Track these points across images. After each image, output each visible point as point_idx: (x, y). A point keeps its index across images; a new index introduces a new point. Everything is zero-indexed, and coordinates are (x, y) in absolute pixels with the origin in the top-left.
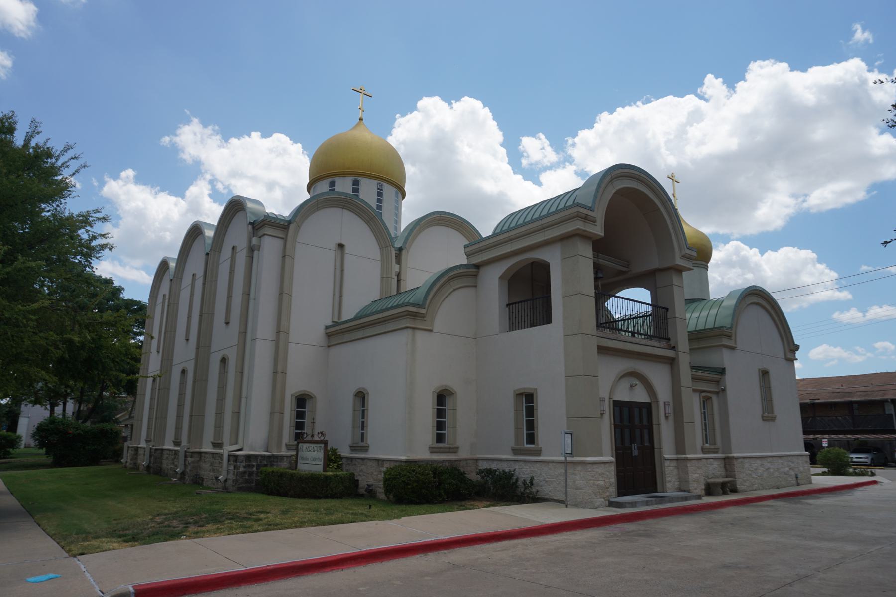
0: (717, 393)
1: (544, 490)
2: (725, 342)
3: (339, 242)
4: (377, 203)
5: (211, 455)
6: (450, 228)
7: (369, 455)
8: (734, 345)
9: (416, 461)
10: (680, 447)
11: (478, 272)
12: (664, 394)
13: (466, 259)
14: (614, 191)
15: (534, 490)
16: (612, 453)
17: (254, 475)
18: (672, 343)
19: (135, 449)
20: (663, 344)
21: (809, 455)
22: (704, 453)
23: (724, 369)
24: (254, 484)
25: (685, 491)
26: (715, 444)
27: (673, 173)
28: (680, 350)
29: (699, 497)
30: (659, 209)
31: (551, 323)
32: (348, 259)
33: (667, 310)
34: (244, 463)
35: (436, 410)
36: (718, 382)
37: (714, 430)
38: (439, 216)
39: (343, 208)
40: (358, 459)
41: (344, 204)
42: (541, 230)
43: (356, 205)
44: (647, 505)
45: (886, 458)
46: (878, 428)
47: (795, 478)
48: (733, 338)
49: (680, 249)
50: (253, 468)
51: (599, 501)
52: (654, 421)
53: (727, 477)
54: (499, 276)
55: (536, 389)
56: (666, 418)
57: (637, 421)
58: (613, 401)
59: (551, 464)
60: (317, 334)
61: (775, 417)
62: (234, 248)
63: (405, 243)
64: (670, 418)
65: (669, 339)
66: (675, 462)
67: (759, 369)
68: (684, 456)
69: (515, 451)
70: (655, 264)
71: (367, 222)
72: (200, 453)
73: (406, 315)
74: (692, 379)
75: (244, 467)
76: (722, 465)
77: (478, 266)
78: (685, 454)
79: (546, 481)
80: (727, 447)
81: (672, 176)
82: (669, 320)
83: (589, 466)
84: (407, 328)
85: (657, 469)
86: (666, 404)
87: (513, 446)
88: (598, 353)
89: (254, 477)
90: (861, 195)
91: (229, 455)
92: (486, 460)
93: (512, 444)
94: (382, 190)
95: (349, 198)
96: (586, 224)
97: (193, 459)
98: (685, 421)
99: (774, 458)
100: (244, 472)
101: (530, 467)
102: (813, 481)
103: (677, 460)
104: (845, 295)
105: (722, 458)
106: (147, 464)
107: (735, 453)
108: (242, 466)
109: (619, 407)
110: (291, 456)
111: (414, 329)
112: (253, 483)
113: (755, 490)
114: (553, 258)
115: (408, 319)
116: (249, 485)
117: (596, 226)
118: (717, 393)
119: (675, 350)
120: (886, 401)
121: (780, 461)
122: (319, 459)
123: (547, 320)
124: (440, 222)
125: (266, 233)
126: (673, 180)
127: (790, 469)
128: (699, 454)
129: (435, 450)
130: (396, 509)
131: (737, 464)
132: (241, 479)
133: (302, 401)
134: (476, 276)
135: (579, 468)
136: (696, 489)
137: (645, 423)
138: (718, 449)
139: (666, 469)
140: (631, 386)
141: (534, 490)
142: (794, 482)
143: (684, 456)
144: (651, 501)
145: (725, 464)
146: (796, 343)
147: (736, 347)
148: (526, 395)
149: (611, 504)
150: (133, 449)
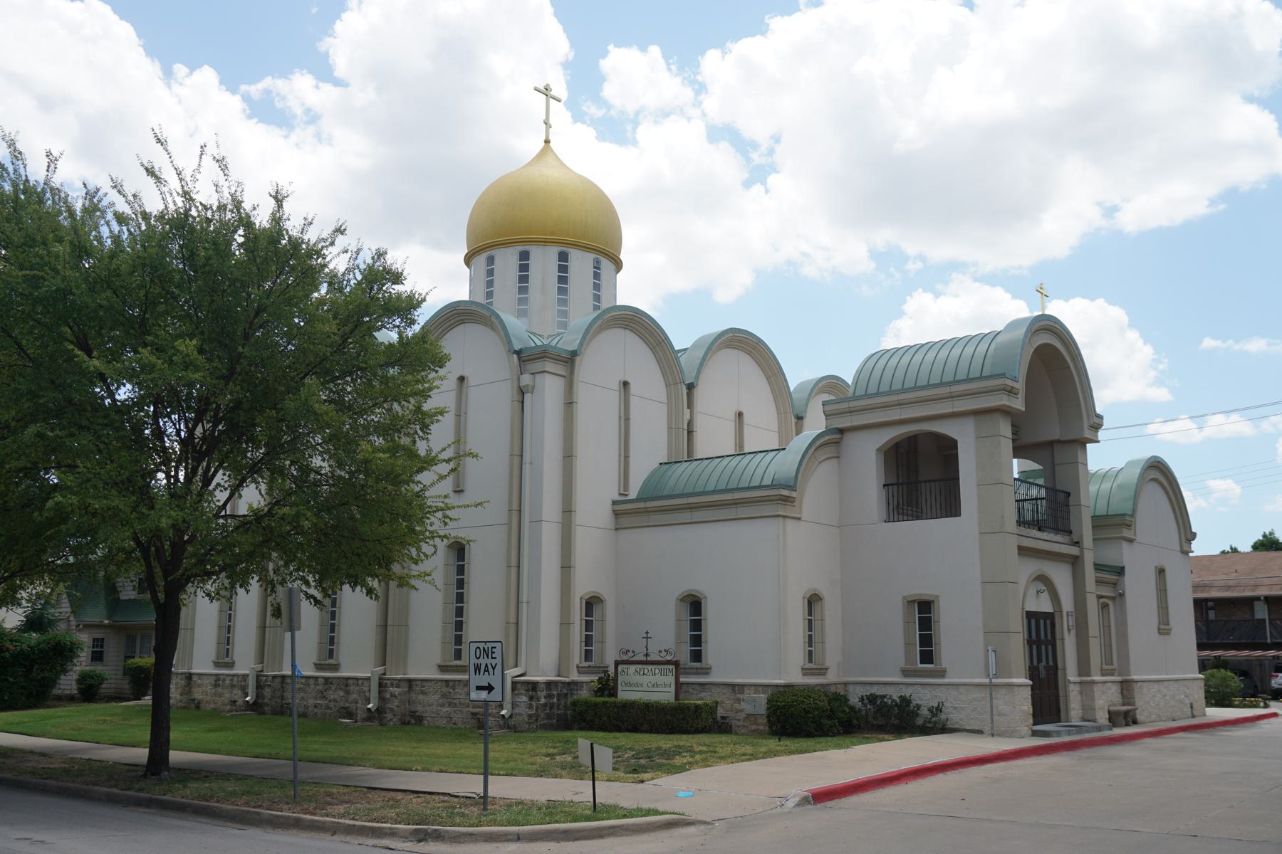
0: (1113, 598)
1: (953, 719)
2: (1126, 533)
3: (623, 379)
4: (558, 283)
5: (444, 683)
6: (740, 352)
7: (714, 678)
8: (1132, 537)
9: (792, 686)
10: (1084, 668)
11: (841, 438)
12: (1067, 604)
13: (824, 420)
14: (1033, 350)
15: (943, 717)
16: (1026, 673)
17: (555, 708)
18: (1075, 538)
19: (186, 677)
20: (1066, 539)
21: (1204, 679)
22: (1103, 675)
23: (1123, 568)
24: (555, 721)
25: (1089, 721)
26: (1112, 664)
27: (1042, 284)
28: (1085, 547)
29: (1099, 729)
30: (1069, 367)
31: (960, 516)
32: (634, 402)
33: (1069, 494)
34: (544, 693)
35: (337, 606)
36: (1115, 584)
37: (1111, 646)
38: (732, 335)
39: (625, 328)
40: (692, 684)
41: (627, 323)
42: (948, 398)
43: (641, 324)
44: (1069, 735)
45: (1256, 686)
46: (1244, 641)
47: (1190, 709)
48: (1133, 527)
49: (1088, 416)
50: (553, 698)
51: (1025, 730)
52: (1058, 636)
53: (1124, 705)
54: (877, 447)
55: (938, 596)
56: (1069, 630)
57: (1043, 637)
58: (1026, 611)
59: (961, 687)
60: (603, 514)
61: (1171, 630)
62: (462, 379)
63: (581, 344)
64: (1072, 631)
65: (1070, 532)
66: (1078, 685)
67: (1156, 567)
68: (1089, 678)
69: (905, 673)
70: (1056, 435)
71: (652, 349)
72: (410, 681)
73: (777, 500)
74: (1096, 582)
75: (545, 697)
76: (1119, 690)
77: (841, 431)
78: (1090, 675)
79: (955, 708)
80: (1125, 668)
81: (1041, 288)
82: (1071, 508)
83: (1016, 688)
84: (779, 516)
85: (1061, 693)
86: (1070, 613)
87: (903, 665)
88: (1019, 554)
89: (555, 711)
90: (1200, 208)
91: (512, 682)
92: (860, 683)
93: (902, 663)
94: (599, 268)
95: (637, 315)
96: (1011, 397)
97: (400, 689)
98: (1090, 635)
99: (1171, 682)
100: (545, 705)
101: (930, 692)
102: (1207, 714)
103: (1081, 683)
104: (1162, 394)
105: (1118, 682)
106: (253, 700)
107: (1135, 675)
108: (542, 697)
109: (1030, 616)
110: (592, 681)
111: (785, 517)
112: (554, 719)
113: (1153, 722)
114: (965, 436)
115: (780, 505)
116: (551, 721)
117: (1018, 398)
118: (1113, 598)
119: (1079, 547)
120: (1258, 599)
121: (1176, 686)
122: (148, 710)
123: (951, 507)
124: (732, 343)
125: (547, 369)
126: (1042, 294)
127: (1186, 696)
128: (1099, 676)
129: (807, 671)
130: (772, 743)
131: (1136, 687)
132: (542, 714)
133: (591, 604)
134: (837, 443)
135: (1003, 691)
136: (1101, 718)
137: (1049, 637)
138: (1115, 670)
139: (1071, 695)
140: (1038, 592)
141: (943, 717)
142: (1189, 713)
143: (1089, 678)
144: (1072, 730)
145: (1122, 689)
146: (1193, 530)
147: (1135, 540)
148: (919, 603)
149: (1035, 734)
150: (183, 676)
